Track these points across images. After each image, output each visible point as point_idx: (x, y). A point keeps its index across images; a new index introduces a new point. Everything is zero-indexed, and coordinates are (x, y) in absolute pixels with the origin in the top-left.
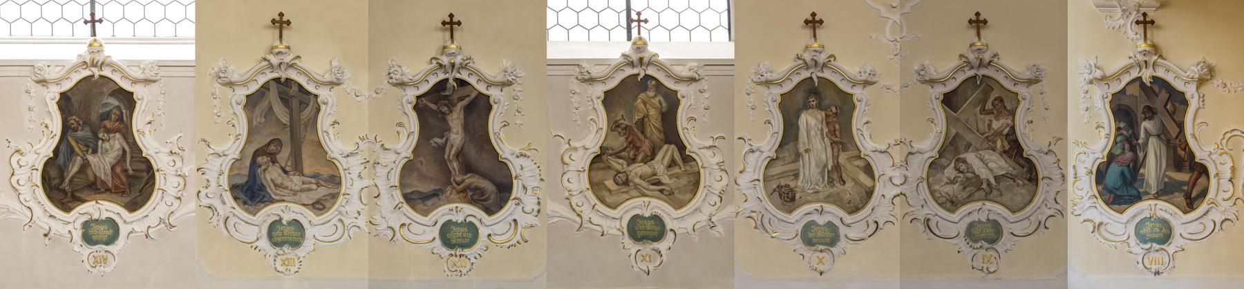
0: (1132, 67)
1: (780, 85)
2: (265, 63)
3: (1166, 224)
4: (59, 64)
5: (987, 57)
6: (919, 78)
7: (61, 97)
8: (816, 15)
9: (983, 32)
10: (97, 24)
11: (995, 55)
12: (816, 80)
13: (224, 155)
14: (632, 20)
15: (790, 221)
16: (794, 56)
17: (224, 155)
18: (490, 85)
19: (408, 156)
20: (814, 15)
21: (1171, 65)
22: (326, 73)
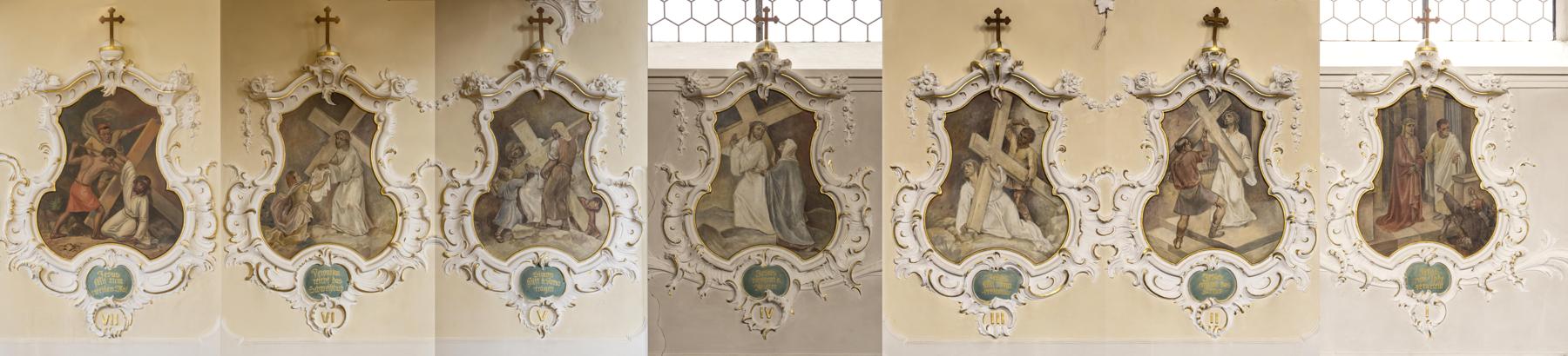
0: (91, 75)
1: (949, 100)
2: (1192, 71)
3: (124, 272)
4: (1378, 72)
5: (1223, 63)
6: (918, 92)
7: (284, 119)
8: (1001, 12)
9: (1003, 34)
10: (1432, 24)
11: (1235, 61)
12: (542, 94)
13: (690, 186)
14: (763, 19)
15: (69, 269)
16: (1185, 62)
17: (690, 186)
18: (1263, 97)
19: (1368, 186)
20: (1217, 11)
21: (142, 73)
22: (1057, 83)
